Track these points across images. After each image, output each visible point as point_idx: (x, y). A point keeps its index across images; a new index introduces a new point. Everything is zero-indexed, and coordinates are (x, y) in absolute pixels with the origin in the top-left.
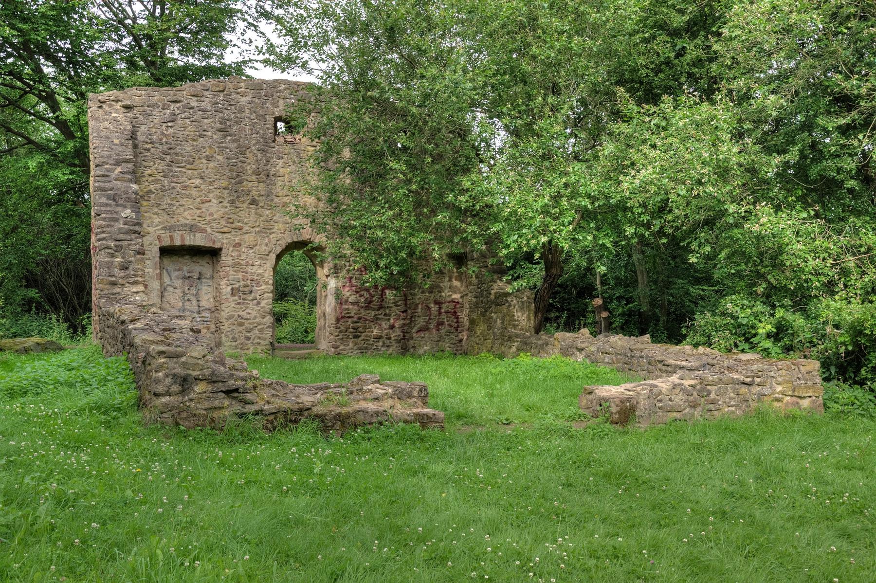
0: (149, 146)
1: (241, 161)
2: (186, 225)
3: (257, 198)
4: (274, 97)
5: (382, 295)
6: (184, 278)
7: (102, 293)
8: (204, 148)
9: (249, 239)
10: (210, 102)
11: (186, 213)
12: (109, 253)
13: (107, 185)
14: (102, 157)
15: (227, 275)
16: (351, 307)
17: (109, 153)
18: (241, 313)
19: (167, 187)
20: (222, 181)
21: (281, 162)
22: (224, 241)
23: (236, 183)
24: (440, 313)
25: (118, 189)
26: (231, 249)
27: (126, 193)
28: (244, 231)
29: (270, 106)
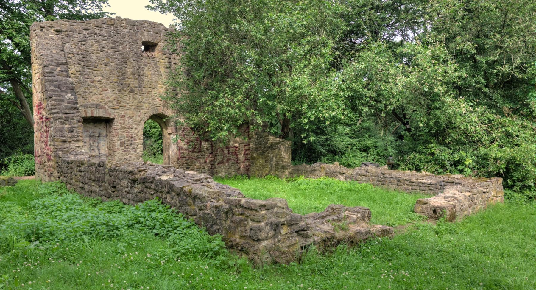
0: (71, 56)
1: (124, 67)
2: (94, 104)
3: (133, 88)
4: (142, 30)
5: (200, 144)
6: (90, 136)
7: (58, 148)
8: (103, 58)
9: (129, 112)
10: (106, 31)
11: (94, 97)
12: (61, 122)
13: (53, 78)
14: (48, 61)
15: (118, 134)
16: (185, 151)
17: (51, 58)
18: (126, 157)
19: (82, 81)
20: (114, 78)
21: (146, 68)
22: (116, 114)
23: (122, 80)
24: (229, 153)
25: (61, 81)
26: (120, 119)
27: (66, 83)
28: (126, 108)
29: (139, 35)
